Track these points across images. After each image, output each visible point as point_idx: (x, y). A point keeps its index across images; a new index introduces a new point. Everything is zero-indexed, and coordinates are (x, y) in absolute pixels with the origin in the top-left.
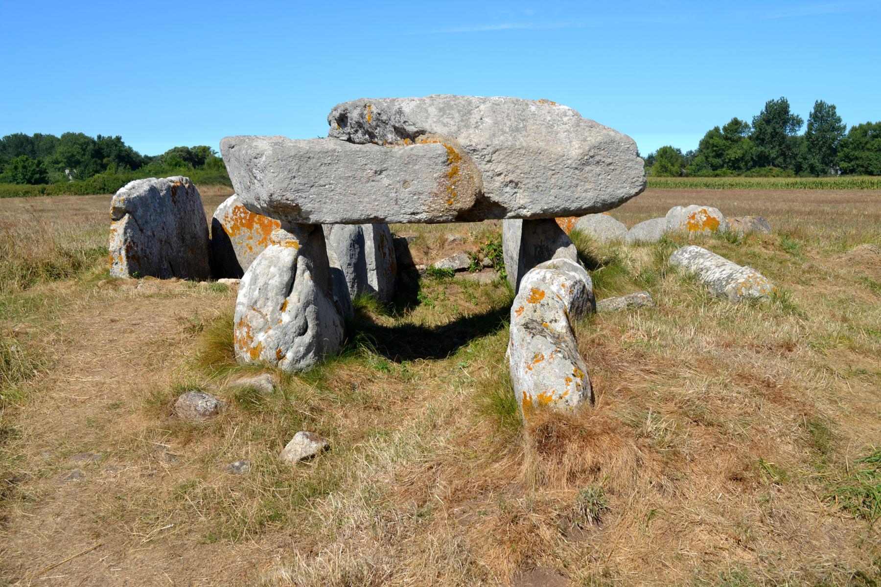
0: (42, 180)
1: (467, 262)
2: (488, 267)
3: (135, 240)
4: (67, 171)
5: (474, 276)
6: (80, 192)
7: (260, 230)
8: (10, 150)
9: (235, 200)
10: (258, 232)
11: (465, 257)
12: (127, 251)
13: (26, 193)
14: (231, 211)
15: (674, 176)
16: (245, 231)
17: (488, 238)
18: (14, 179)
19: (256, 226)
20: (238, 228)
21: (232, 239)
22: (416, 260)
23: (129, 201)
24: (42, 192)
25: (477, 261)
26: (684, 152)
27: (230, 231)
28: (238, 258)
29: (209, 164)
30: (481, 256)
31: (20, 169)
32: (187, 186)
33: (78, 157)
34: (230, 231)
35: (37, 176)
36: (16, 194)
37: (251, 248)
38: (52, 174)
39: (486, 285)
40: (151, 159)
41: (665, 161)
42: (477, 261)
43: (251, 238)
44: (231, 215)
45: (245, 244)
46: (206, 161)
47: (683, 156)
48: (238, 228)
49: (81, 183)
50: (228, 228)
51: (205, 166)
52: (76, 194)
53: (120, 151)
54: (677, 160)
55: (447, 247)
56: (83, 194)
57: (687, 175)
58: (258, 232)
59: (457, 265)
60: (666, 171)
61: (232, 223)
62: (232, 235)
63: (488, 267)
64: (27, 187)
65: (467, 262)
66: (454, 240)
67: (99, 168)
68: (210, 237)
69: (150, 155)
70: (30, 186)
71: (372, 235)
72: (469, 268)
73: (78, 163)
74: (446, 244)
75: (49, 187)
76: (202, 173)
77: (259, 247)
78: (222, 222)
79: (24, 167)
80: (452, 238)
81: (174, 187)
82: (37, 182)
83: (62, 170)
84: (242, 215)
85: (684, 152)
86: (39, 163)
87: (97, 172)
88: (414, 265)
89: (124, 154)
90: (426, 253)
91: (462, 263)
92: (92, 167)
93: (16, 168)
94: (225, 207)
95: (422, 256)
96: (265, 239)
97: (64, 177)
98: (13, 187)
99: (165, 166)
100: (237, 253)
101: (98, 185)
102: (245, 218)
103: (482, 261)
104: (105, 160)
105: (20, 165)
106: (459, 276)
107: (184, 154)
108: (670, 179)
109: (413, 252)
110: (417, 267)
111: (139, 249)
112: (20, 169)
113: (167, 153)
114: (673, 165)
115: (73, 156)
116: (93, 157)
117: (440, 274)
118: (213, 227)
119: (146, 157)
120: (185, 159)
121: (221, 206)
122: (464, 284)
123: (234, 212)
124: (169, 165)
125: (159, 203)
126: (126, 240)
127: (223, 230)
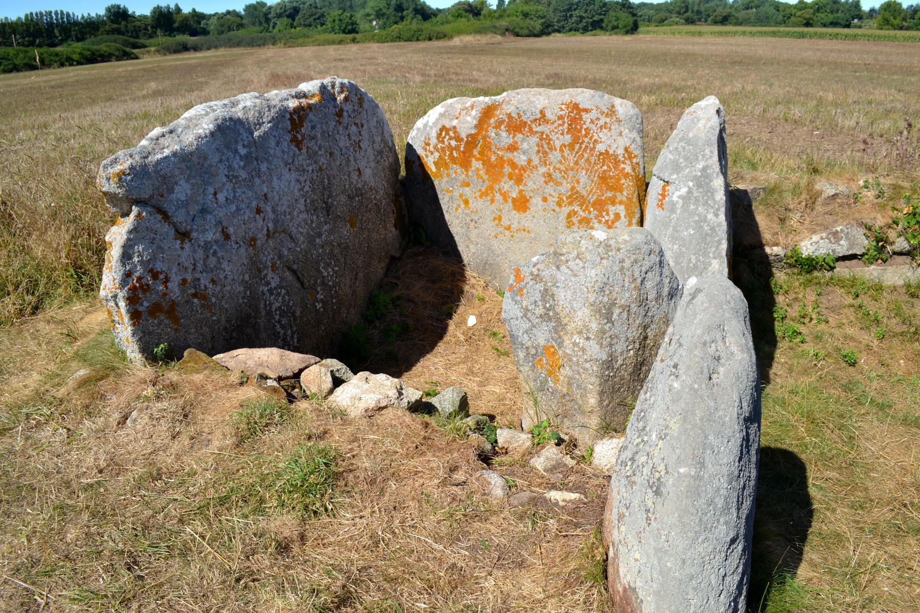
0: (353, 31)
1: (862, 243)
2: (901, 254)
3: (159, 266)
4: (374, 23)
5: (872, 272)
6: (382, 40)
7: (481, 172)
8: (334, 5)
9: (442, 115)
10: (479, 176)
11: (859, 234)
12: (132, 300)
13: (341, 42)
14: (434, 133)
15: (895, 29)
16: (456, 170)
17: (908, 199)
18: (333, 30)
19: (476, 164)
20: (446, 166)
21: (436, 183)
22: (766, 236)
23: (139, 173)
24: (354, 41)
25: (881, 242)
26: (905, 6)
27: (434, 169)
28: (447, 217)
29: (485, 16)
30: (892, 234)
31: (337, 22)
32: (340, 98)
33: (384, 10)
34: (434, 169)
35: (350, 27)
36: (333, 42)
37: (466, 202)
38: (363, 25)
39: (895, 288)
40: (439, 11)
41: (887, 15)
42: (881, 242)
43: (468, 185)
44: (434, 141)
45: (456, 194)
46: (483, 12)
47: (903, 10)
48: (446, 166)
49: (384, 33)
50: (430, 162)
51: (481, 17)
52: (378, 42)
53: (416, 5)
54: (900, 14)
55: (819, 208)
56: (384, 42)
57: (908, 29)
58: (479, 176)
59: (843, 249)
60: (888, 24)
61: (437, 155)
62: (436, 175)
63: (901, 254)
64: (342, 36)
65: (862, 243)
66: (835, 196)
67: (398, 19)
68: (403, 173)
69: (441, 7)
70: (344, 35)
71: (724, 246)
72: (862, 255)
73: (383, 15)
74: (820, 200)
75: (358, 36)
76: (479, 22)
77: (481, 202)
78: (420, 151)
79: (340, 20)
80: (831, 191)
81: (299, 110)
82: (350, 32)
83: (371, 21)
84: (453, 143)
85: (905, 6)
86: (351, 16)
87: (396, 23)
88: (761, 246)
89: (419, 7)
90: (782, 221)
91: (851, 246)
92: (392, 19)
93: (334, 21)
94: (426, 125)
95: (776, 227)
96: (491, 188)
97: (371, 27)
98: (332, 36)
99: (450, 17)
100: (444, 207)
101: (395, 34)
102: (457, 148)
103: (892, 243)
104: (405, 13)
105: (337, 19)
106: (842, 270)
107: (466, 7)
108: (892, 33)
109: (761, 219)
110: (768, 250)
111: (174, 285)
112: (337, 22)
113: (453, 6)
114: (895, 18)
115: (380, 9)
116: (395, 10)
117: (809, 266)
118: (406, 158)
119: (437, 9)
120: (467, 11)
121: (420, 123)
122: (852, 286)
123: (439, 136)
124: (453, 16)
125: (247, 158)
126: (128, 275)
127: (422, 166)
